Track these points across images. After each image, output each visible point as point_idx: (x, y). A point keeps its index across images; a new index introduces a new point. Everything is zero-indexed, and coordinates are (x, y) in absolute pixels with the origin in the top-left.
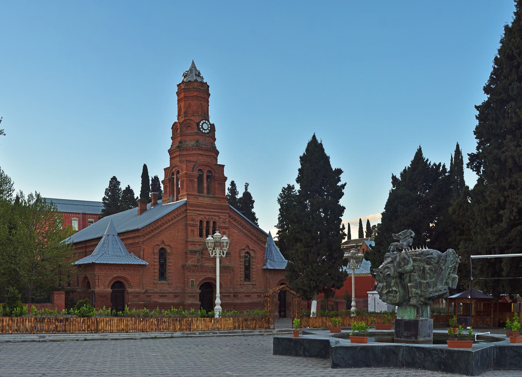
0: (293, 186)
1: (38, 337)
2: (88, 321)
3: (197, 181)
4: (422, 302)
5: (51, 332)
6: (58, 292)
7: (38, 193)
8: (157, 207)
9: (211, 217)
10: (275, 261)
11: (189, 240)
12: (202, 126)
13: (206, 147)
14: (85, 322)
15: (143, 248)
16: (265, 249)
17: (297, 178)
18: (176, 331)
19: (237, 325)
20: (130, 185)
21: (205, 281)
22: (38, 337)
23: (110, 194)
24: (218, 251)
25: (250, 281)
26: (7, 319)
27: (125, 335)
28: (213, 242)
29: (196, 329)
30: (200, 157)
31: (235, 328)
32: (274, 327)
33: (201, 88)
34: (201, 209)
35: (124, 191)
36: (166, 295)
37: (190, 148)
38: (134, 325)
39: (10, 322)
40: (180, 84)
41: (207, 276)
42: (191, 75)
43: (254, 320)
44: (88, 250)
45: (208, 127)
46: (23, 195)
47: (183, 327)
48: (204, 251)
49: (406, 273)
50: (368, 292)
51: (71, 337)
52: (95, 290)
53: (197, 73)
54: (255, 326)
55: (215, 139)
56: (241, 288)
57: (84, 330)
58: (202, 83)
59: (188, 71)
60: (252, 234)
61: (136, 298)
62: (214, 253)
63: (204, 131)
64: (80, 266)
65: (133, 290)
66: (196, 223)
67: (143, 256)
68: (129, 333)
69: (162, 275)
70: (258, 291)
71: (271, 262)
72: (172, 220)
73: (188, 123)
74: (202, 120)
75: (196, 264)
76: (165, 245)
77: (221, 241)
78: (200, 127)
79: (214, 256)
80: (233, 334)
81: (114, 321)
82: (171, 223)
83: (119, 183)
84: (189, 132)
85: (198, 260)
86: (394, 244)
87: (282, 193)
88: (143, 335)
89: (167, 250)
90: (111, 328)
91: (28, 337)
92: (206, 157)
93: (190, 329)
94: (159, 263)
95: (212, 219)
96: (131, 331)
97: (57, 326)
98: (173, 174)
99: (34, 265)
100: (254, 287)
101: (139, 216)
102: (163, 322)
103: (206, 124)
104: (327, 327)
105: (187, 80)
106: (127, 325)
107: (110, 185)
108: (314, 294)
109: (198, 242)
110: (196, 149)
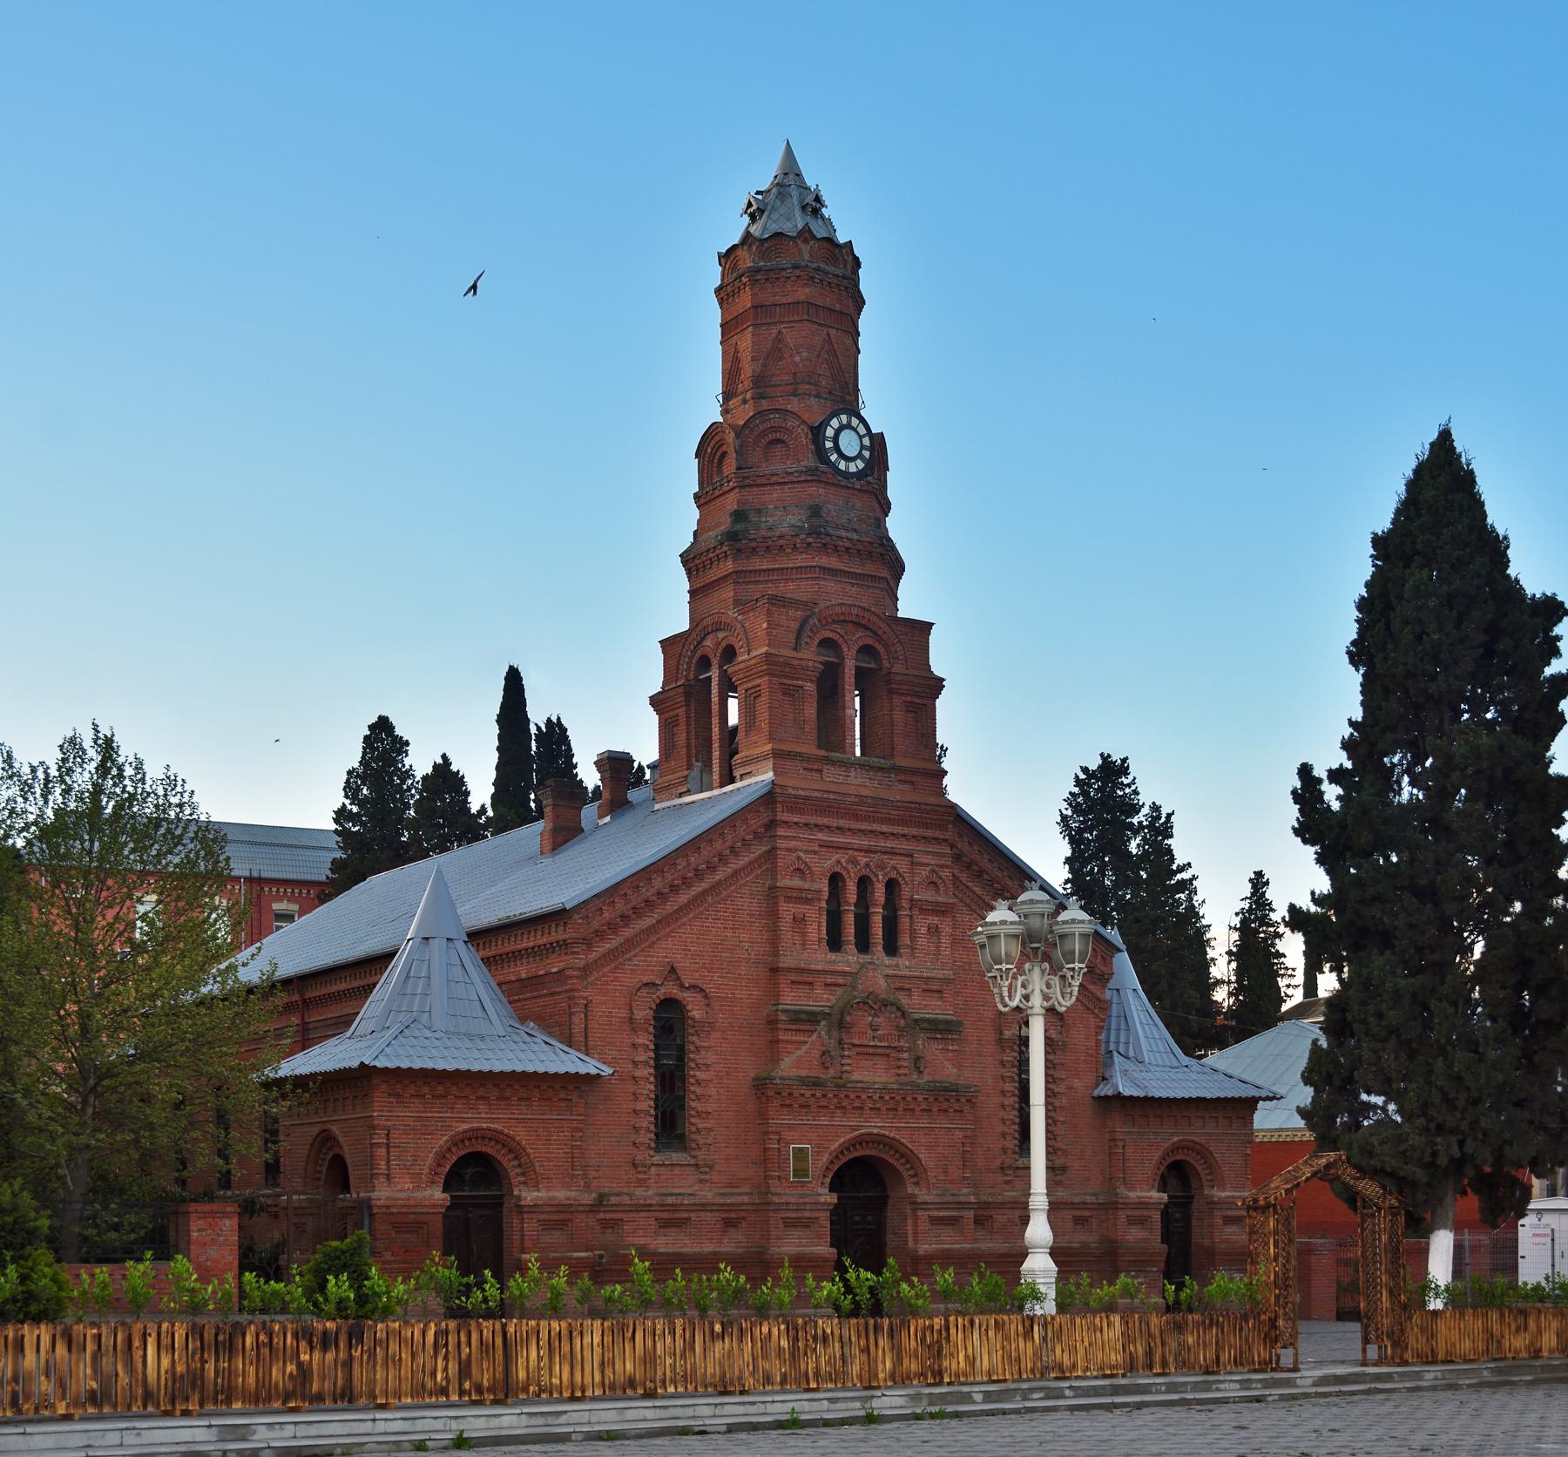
0: (1124, 760)
1: (211, 1435)
2: (463, 1339)
3: (815, 693)
5: (277, 1405)
6: (207, 1207)
7: (105, 731)
8: (628, 819)
10: (1147, 1061)
11: (786, 961)
12: (836, 439)
13: (855, 536)
14: (446, 1345)
15: (584, 998)
17: (1354, 643)
18: (878, 1388)
19: (1140, 1349)
21: (851, 1157)
22: (214, 1431)
23: (365, 791)
26: (45, 1332)
27: (649, 1414)
28: (1017, 936)
29: (965, 1375)
30: (830, 585)
31: (1131, 1367)
32: (1296, 1362)
33: (827, 268)
34: (834, 823)
35: (425, 778)
36: (689, 1219)
37: (781, 542)
38: (683, 1356)
39: (61, 1349)
40: (734, 247)
42: (783, 210)
43: (1211, 1325)
44: (315, 1017)
45: (863, 447)
46: (17, 765)
47: (906, 1361)
48: (849, 1013)
51: (381, 1427)
52: (375, 1195)
53: (810, 199)
54: (1218, 1358)
56: (1007, 1182)
57: (444, 1391)
59: (769, 191)
61: (557, 1233)
62: (1020, 992)
63: (842, 465)
64: (301, 1082)
66: (815, 886)
67: (586, 1037)
68: (658, 1403)
70: (1077, 1200)
71: (1128, 1065)
72: (712, 868)
75: (813, 1074)
76: (682, 986)
77: (1058, 929)
78: (829, 445)
80: (1137, 1398)
81: (587, 1340)
82: (704, 885)
83: (401, 745)
84: (778, 467)
85: (824, 1053)
87: (1076, 790)
88: (734, 1409)
90: (572, 1374)
91: (159, 1436)
92: (853, 585)
93: (940, 1373)
94: (656, 1068)
95: (881, 867)
96: (671, 1389)
97: (304, 1371)
98: (705, 663)
99: (92, 1082)
100: (1058, 1178)
101: (548, 860)
102: (815, 1338)
103: (853, 433)
104: (1506, 1358)
105: (765, 228)
106: (649, 1359)
107: (364, 754)
108: (1440, 1200)
109: (824, 972)
110: (809, 544)
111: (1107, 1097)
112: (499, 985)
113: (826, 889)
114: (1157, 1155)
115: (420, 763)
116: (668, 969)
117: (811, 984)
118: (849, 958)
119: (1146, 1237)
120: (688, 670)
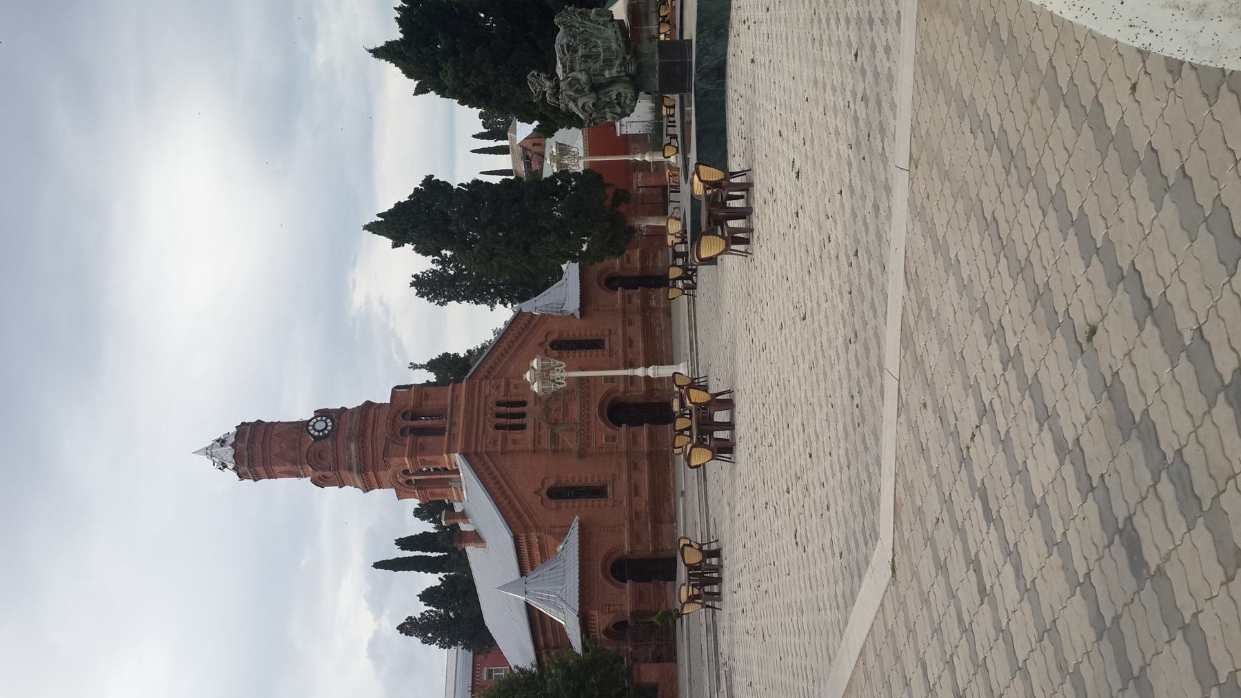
4: (631, 58)
9: (488, 411)
11: (530, 446)
12: (319, 431)
20: (377, 213)
24: (557, 375)
25: (604, 340)
40: (238, 474)
41: (597, 413)
45: (321, 420)
49: (591, 80)
50: (618, 135)
55: (343, 408)
56: (616, 354)
58: (237, 435)
62: (560, 381)
63: (329, 428)
69: (598, 492)
73: (315, 457)
74: (309, 431)
76: (542, 489)
86: (548, 99)
89: (550, 485)
98: (409, 482)
116: (535, 495)
117: (539, 436)
118: (529, 421)
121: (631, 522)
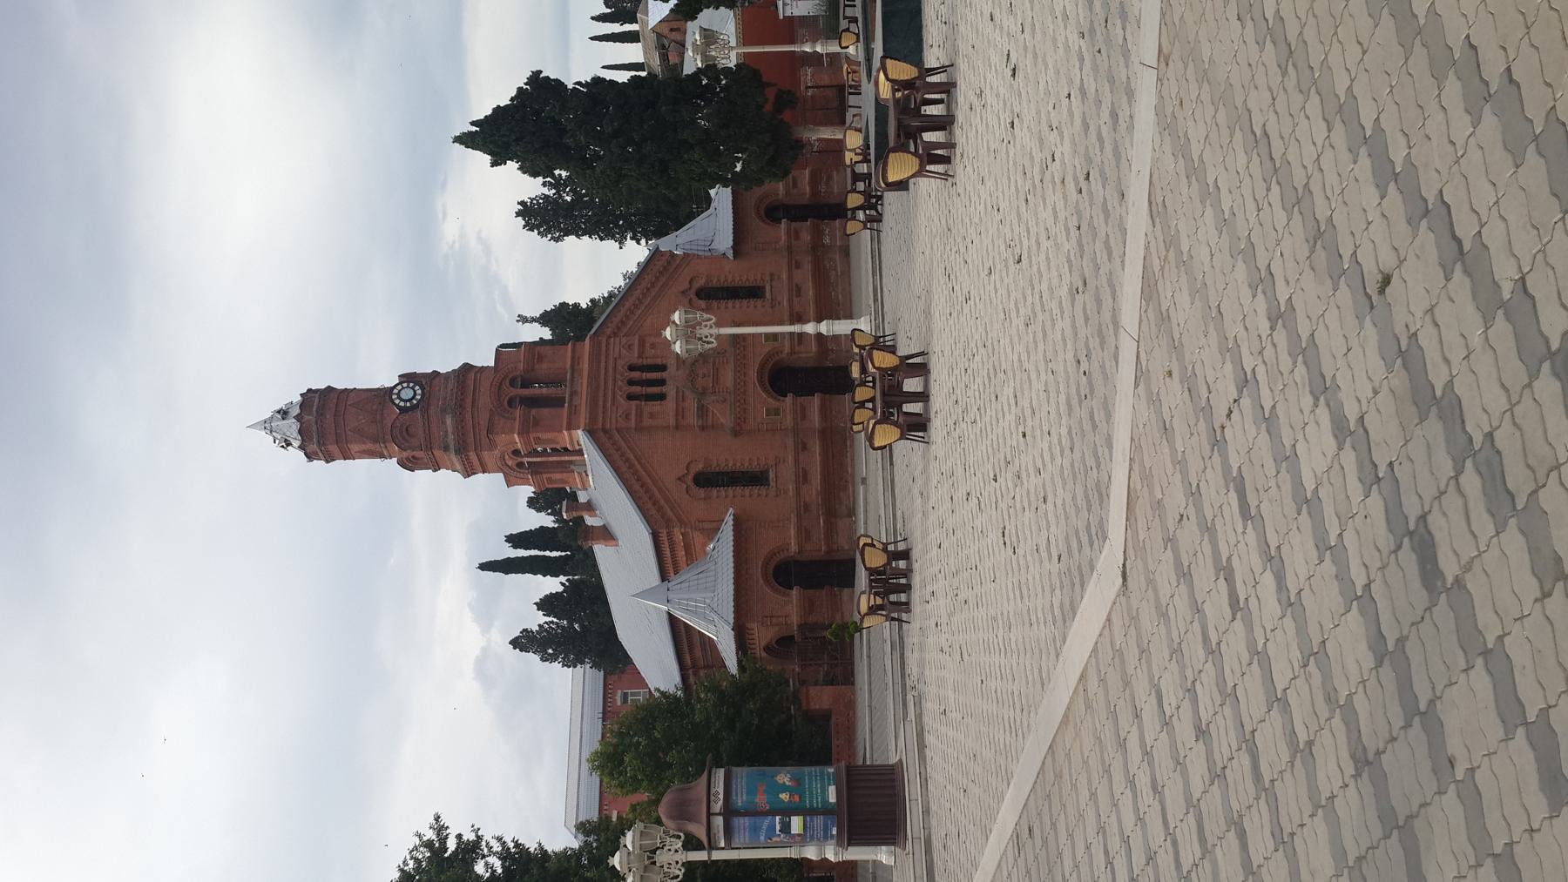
11: (672, 422)
12: (406, 401)
16: (688, 254)
21: (767, 384)
34: (601, 399)
35: (530, 169)
40: (305, 454)
41: (756, 382)
45: (408, 387)
50: (781, 17)
55: (435, 372)
56: (779, 304)
60: (653, 285)
62: (708, 339)
63: (418, 397)
65: (793, 542)
66: (634, 408)
69: (756, 479)
72: (627, 460)
73: (401, 433)
74: (392, 401)
79: (715, 339)
98: (520, 465)
100: (776, 277)
111: (734, 253)
112: (688, 565)
113: (635, 402)
114: (763, 225)
115: (537, 619)
117: (683, 409)
118: (670, 390)
119: (805, 229)
120: (523, 473)
121: (799, 517)
